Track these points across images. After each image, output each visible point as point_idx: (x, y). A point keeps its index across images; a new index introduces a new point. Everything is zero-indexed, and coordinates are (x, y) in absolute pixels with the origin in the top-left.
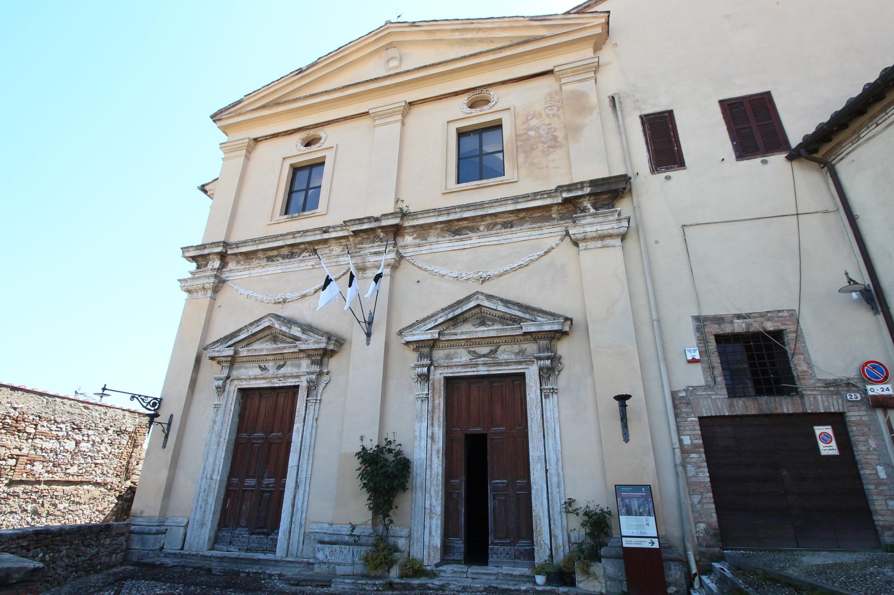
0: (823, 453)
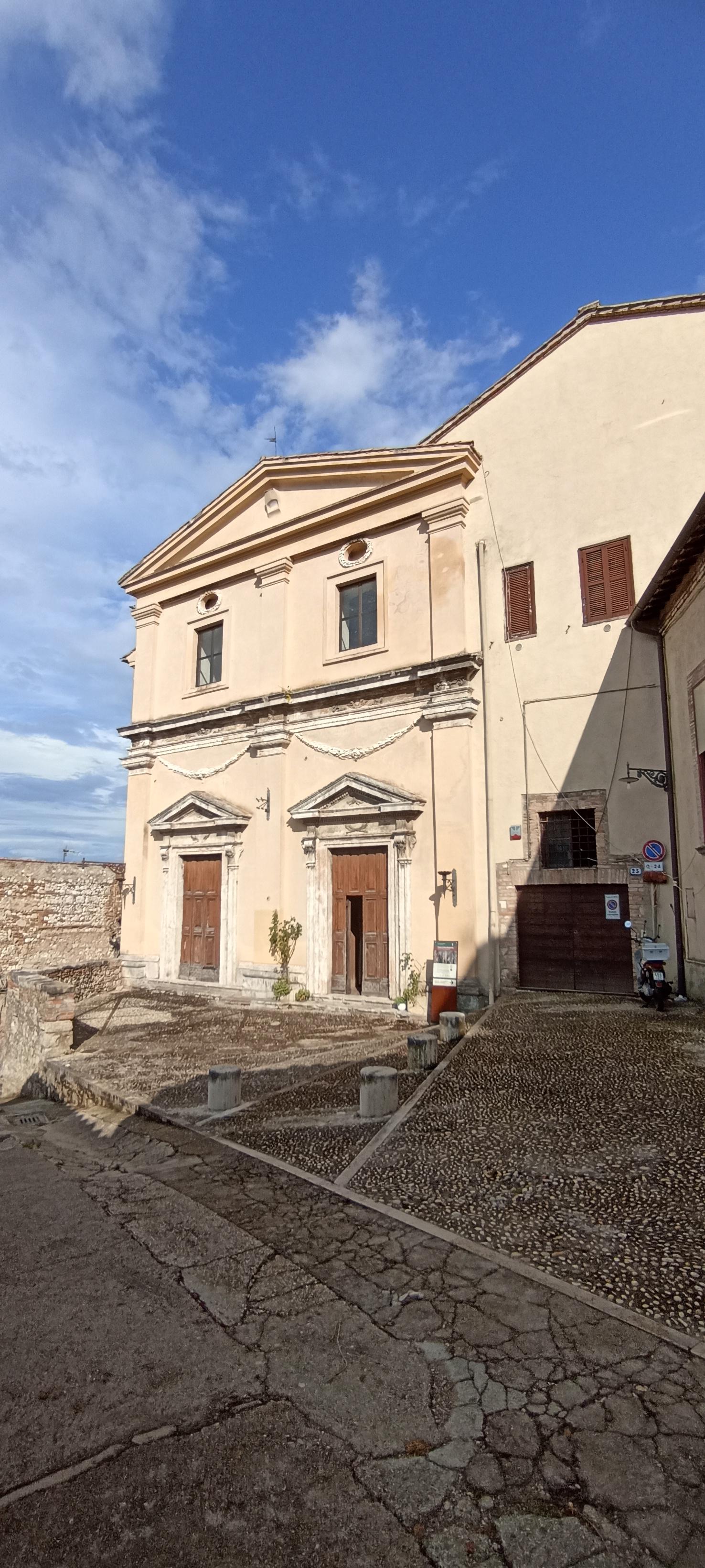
0: (608, 917)
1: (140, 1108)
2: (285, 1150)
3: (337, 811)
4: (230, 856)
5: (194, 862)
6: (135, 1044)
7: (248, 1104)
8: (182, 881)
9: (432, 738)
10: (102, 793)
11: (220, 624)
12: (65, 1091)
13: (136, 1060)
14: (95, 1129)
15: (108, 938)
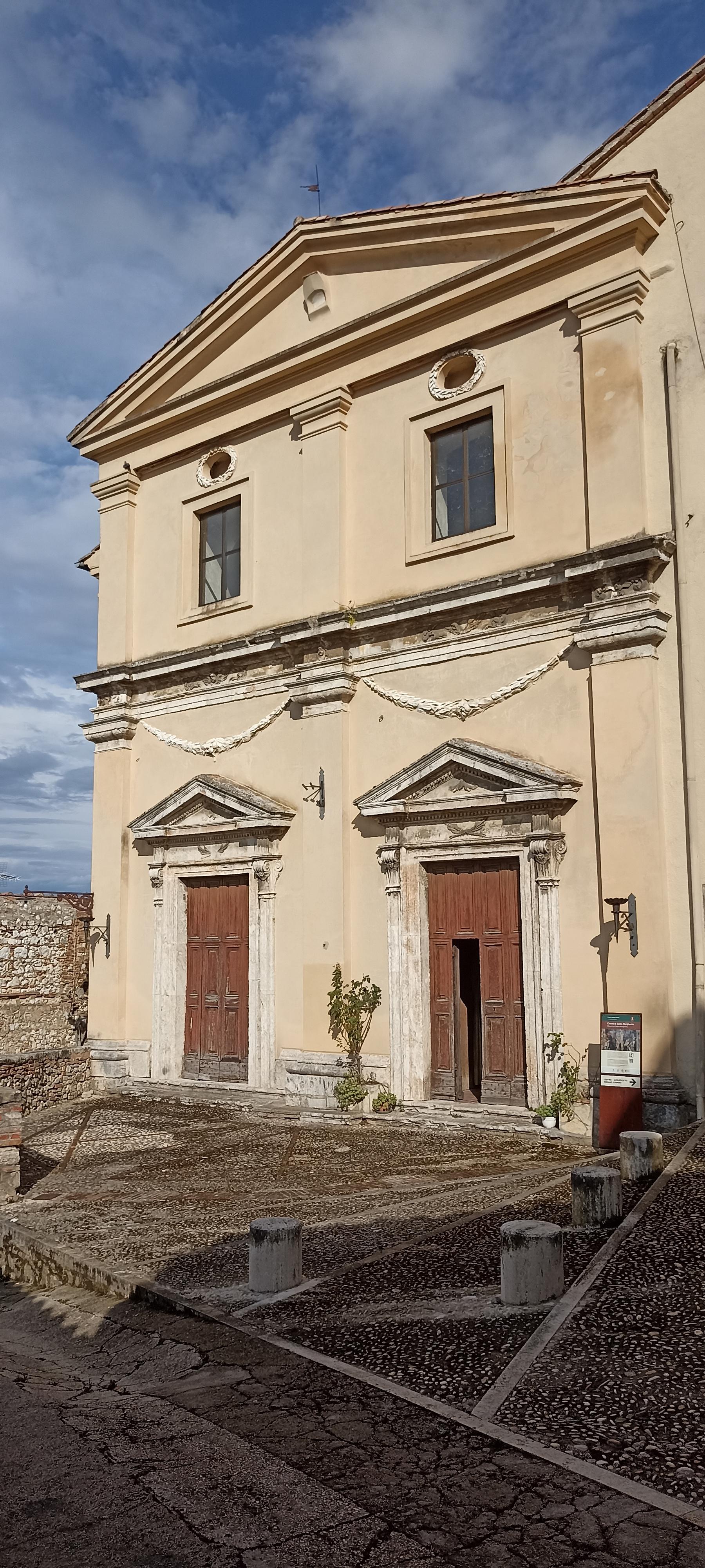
1: (138, 1288)
2: (385, 1358)
3: (434, 802)
4: (261, 877)
5: (204, 889)
6: (119, 1183)
7: (314, 1282)
8: (184, 918)
9: (590, 680)
10: (44, 779)
11: (236, 502)
12: (12, 1262)
13: (123, 1210)
14: (66, 1324)
15: (66, 1014)
